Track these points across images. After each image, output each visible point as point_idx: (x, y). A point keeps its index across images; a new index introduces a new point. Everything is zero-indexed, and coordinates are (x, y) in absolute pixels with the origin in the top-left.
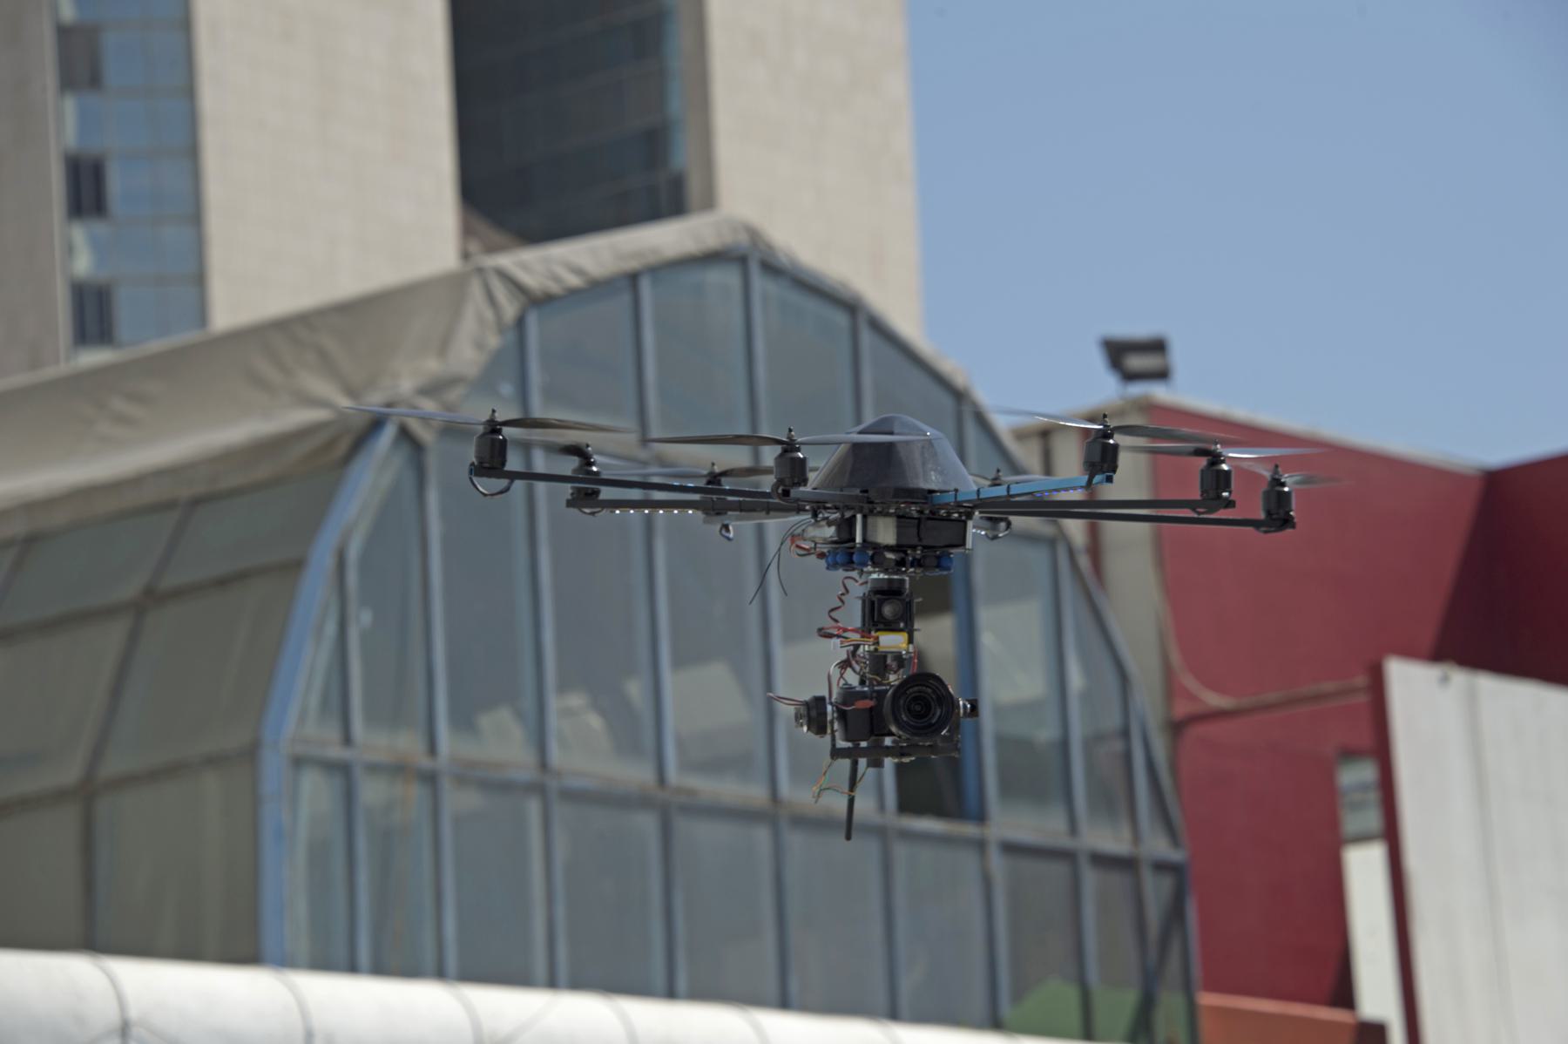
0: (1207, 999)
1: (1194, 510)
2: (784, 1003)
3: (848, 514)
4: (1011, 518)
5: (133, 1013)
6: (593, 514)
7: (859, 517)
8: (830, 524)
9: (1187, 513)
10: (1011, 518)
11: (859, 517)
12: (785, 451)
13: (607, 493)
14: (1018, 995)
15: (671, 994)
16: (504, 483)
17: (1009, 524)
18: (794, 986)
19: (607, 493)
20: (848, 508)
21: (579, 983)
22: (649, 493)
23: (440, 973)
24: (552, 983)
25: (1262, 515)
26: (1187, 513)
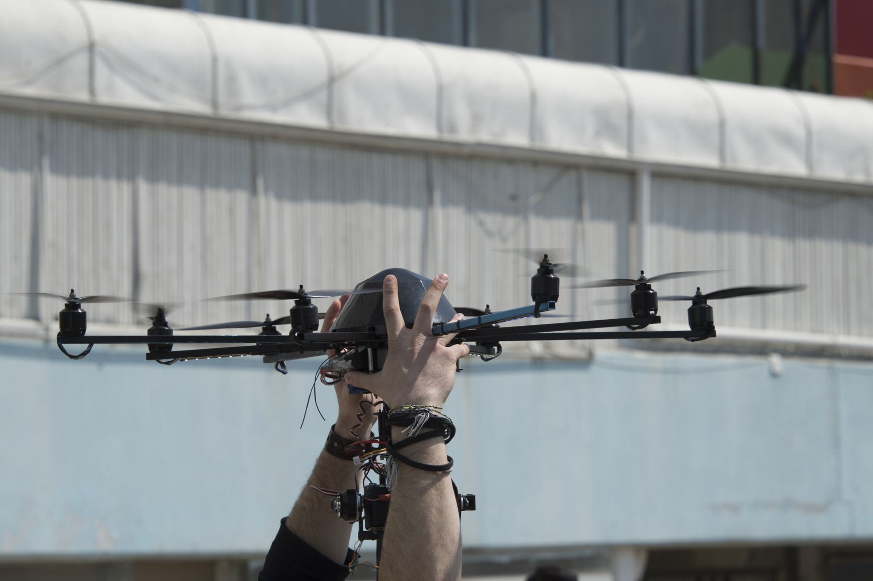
0: (841, 59)
1: (629, 326)
2: (544, 52)
3: (360, 349)
4: (500, 343)
5: (97, 36)
6: (168, 363)
7: (369, 350)
8: (347, 359)
9: (624, 329)
10: (500, 343)
11: (369, 350)
12: (694, 303)
13: (177, 348)
14: (709, 53)
15: (465, 43)
16: (84, 347)
17: (499, 348)
18: (552, 42)
19: (177, 348)
20: (364, 344)
21: (403, 30)
22: (216, 348)
23: (304, 21)
24: (382, 32)
25: (688, 328)
26: (624, 329)
